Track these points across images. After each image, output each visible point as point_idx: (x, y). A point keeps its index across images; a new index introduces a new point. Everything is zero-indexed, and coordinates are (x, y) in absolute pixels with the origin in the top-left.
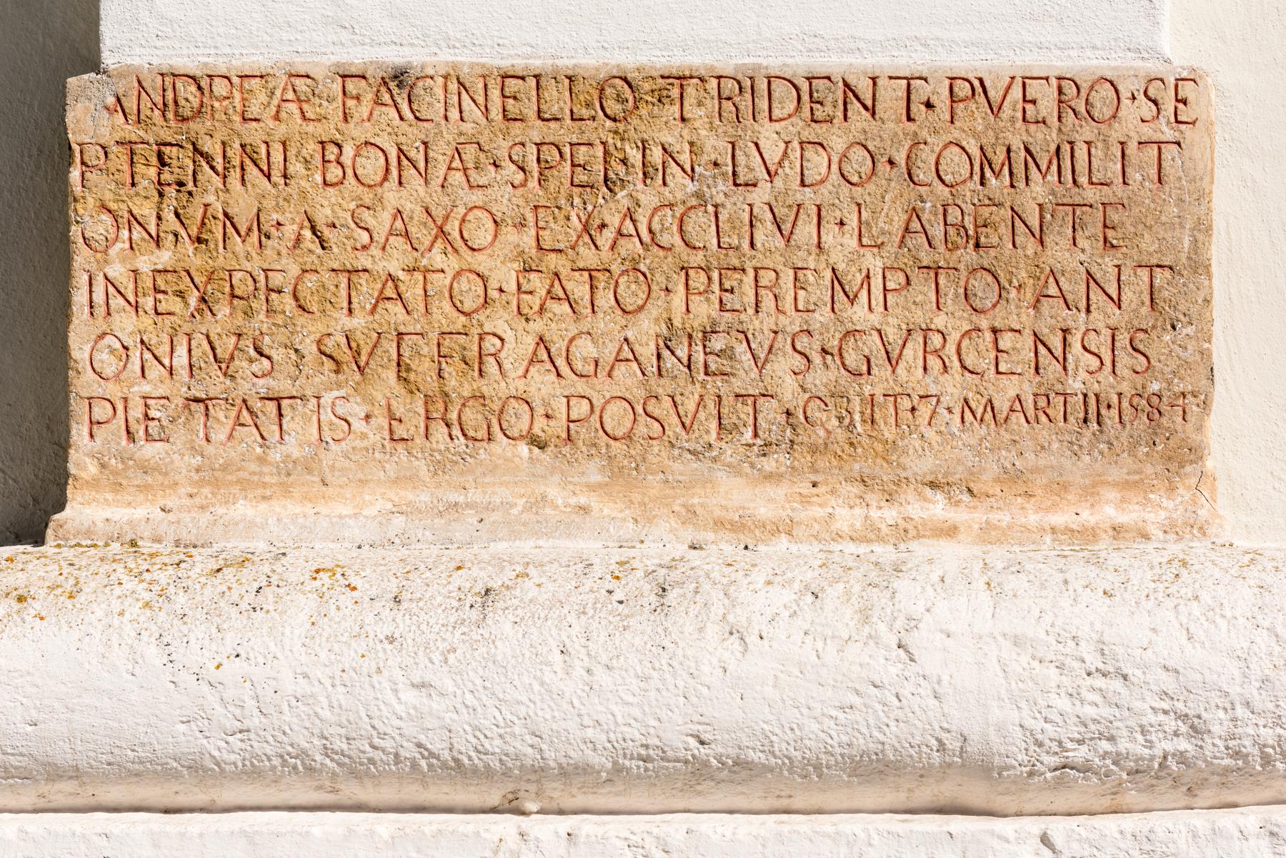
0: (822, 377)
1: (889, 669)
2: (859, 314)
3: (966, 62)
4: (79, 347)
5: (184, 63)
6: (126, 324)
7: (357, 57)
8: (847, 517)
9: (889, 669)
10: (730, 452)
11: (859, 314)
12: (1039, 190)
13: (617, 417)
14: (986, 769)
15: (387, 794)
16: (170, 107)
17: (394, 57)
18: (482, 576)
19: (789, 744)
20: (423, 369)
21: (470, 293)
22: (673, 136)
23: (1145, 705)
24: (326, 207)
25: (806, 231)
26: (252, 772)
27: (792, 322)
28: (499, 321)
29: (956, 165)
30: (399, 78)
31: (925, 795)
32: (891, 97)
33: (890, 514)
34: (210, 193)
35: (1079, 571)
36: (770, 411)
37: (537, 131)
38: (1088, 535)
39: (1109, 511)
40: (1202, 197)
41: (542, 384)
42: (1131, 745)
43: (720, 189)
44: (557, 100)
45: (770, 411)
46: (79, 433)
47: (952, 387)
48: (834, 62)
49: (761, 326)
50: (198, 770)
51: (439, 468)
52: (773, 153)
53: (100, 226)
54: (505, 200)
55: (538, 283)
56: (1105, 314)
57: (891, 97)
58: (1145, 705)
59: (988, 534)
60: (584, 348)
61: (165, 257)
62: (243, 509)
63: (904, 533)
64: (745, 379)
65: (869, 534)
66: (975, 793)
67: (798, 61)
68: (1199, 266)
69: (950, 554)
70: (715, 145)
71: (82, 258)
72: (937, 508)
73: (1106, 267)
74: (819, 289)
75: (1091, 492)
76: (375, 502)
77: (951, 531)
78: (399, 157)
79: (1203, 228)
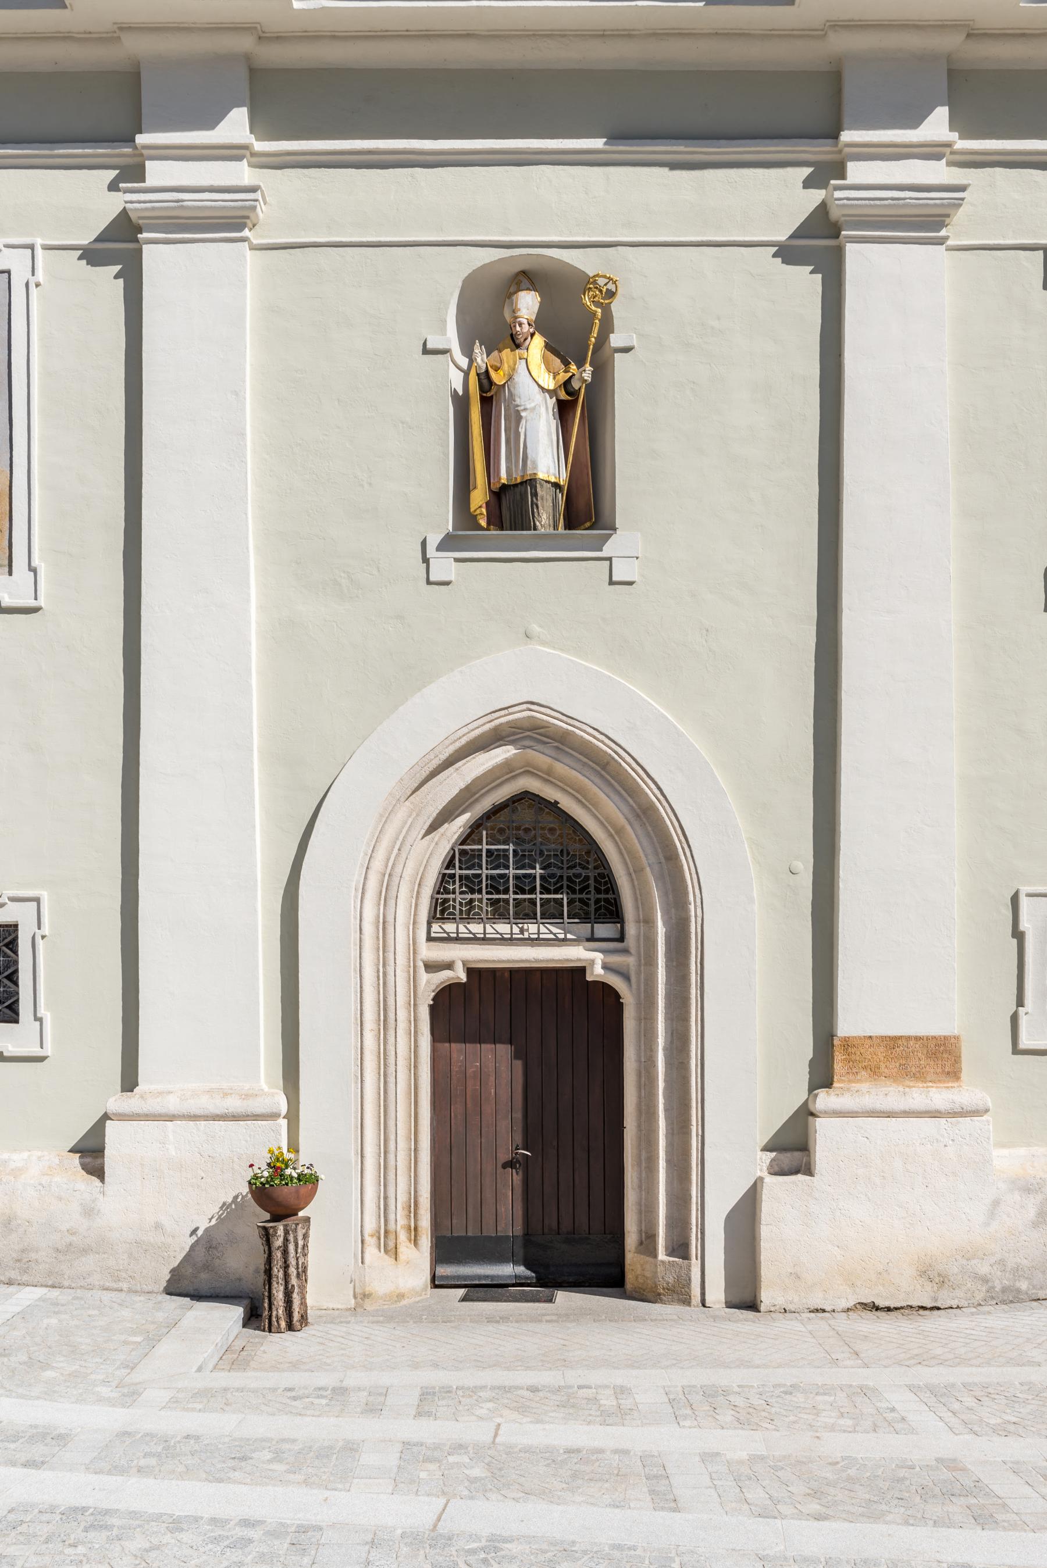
0: (917, 1070)
1: (930, 1102)
2: (922, 1062)
3: (933, 1034)
4: (835, 1067)
5: (847, 1036)
6: (840, 1064)
7: (866, 1035)
8: (921, 1085)
9: (930, 1102)
10: (907, 1078)
11: (922, 1062)
12: (942, 1048)
13: (894, 1074)
14: (939, 1112)
15: (876, 1115)
16: (845, 1040)
17: (869, 1035)
18: (183, 1338)
19: (1013, 1551)
20: (873, 1070)
21: (878, 1060)
22: (901, 1043)
23: (957, 1106)
24: (862, 1051)
25: (916, 1053)
26: (863, 1113)
27: (914, 1063)
28: (881, 1064)
29: (932, 1046)
30: (870, 1037)
31: (933, 1115)
32: (925, 1039)
33: (925, 1085)
34: (850, 1050)
35: (949, 1092)
36: (912, 1073)
37: (885, 1042)
38: (948, 1087)
39: (950, 1085)
40: (960, 1049)
41: (886, 1070)
42: (956, 1110)
43: (906, 1049)
44: (888, 1039)
45: (912, 1073)
46: (835, 1076)
47: (932, 1070)
48: (918, 1034)
49: (911, 1064)
50: (857, 1112)
51: (875, 1080)
52: (912, 1044)
53: (837, 1053)
54: (882, 1050)
55: (886, 1059)
56: (950, 1062)
57: (925, 1039)
58: (957, 1106)
59: (937, 1087)
60: (891, 1066)
61: (844, 1057)
62: (853, 1085)
63: (927, 1087)
64: (909, 1070)
65: (923, 1087)
66: (939, 1115)
67: (914, 1034)
68: (960, 1057)
69: (934, 1089)
70: (905, 1044)
71: (836, 1057)
72: (931, 1084)
73: (950, 1057)
74: (917, 1059)
75: (948, 1082)
76: (868, 1084)
77: (933, 1087)
78: (533, 749)
79: (960, 1052)
